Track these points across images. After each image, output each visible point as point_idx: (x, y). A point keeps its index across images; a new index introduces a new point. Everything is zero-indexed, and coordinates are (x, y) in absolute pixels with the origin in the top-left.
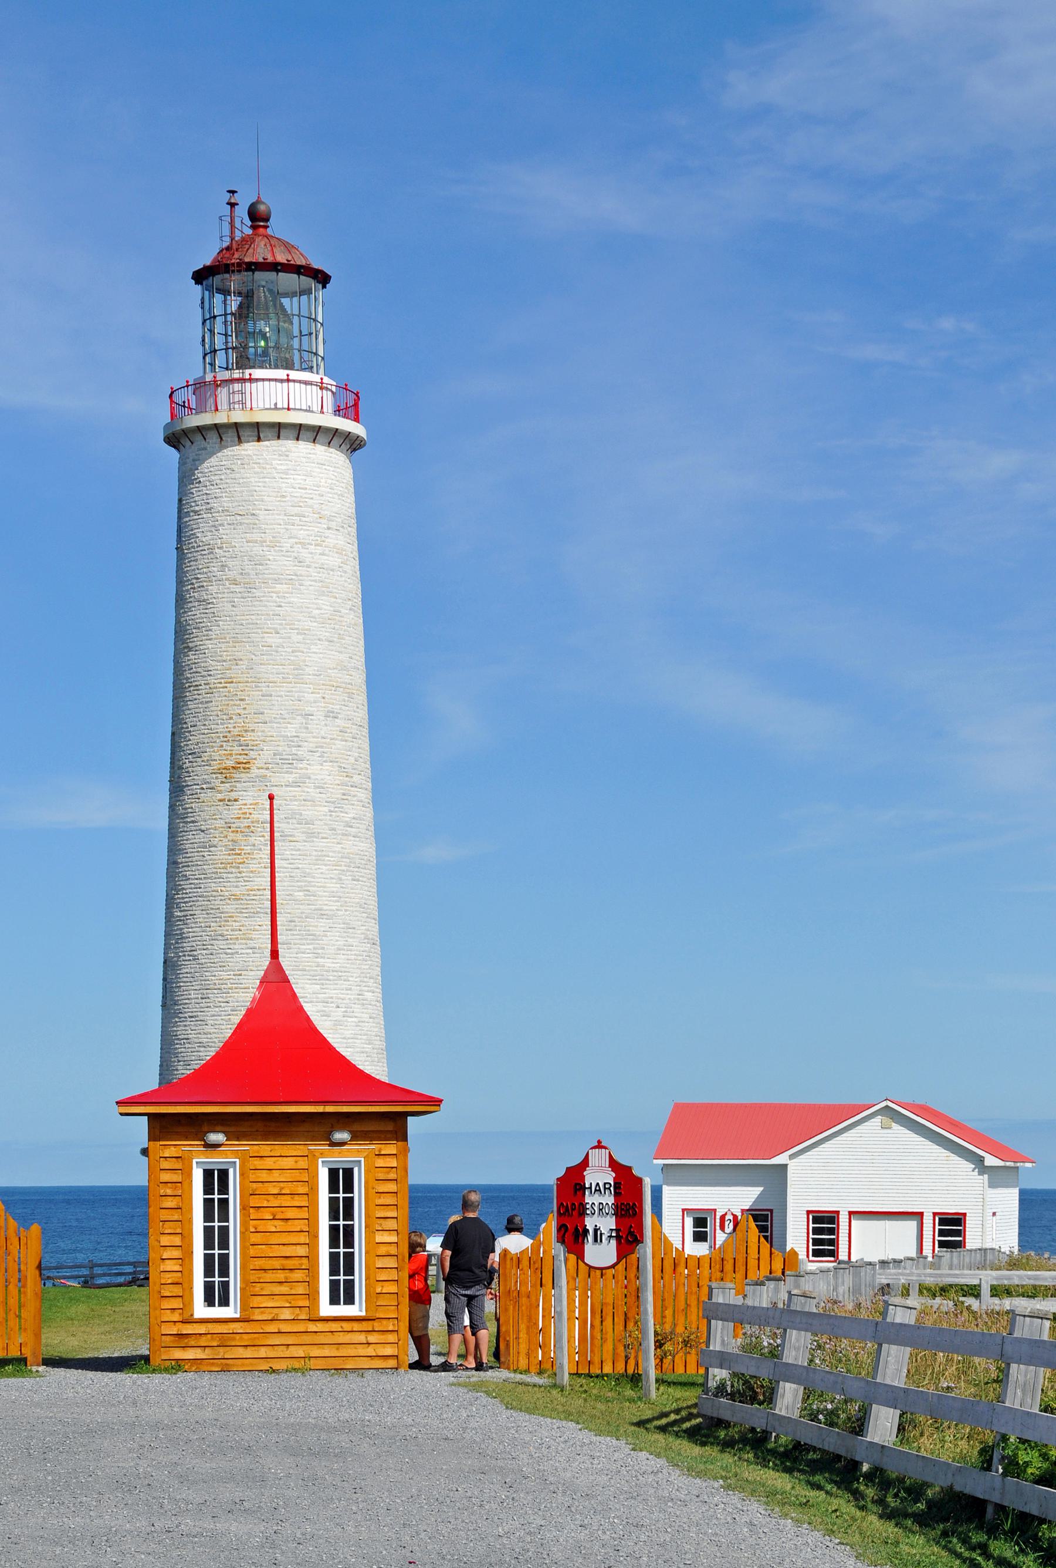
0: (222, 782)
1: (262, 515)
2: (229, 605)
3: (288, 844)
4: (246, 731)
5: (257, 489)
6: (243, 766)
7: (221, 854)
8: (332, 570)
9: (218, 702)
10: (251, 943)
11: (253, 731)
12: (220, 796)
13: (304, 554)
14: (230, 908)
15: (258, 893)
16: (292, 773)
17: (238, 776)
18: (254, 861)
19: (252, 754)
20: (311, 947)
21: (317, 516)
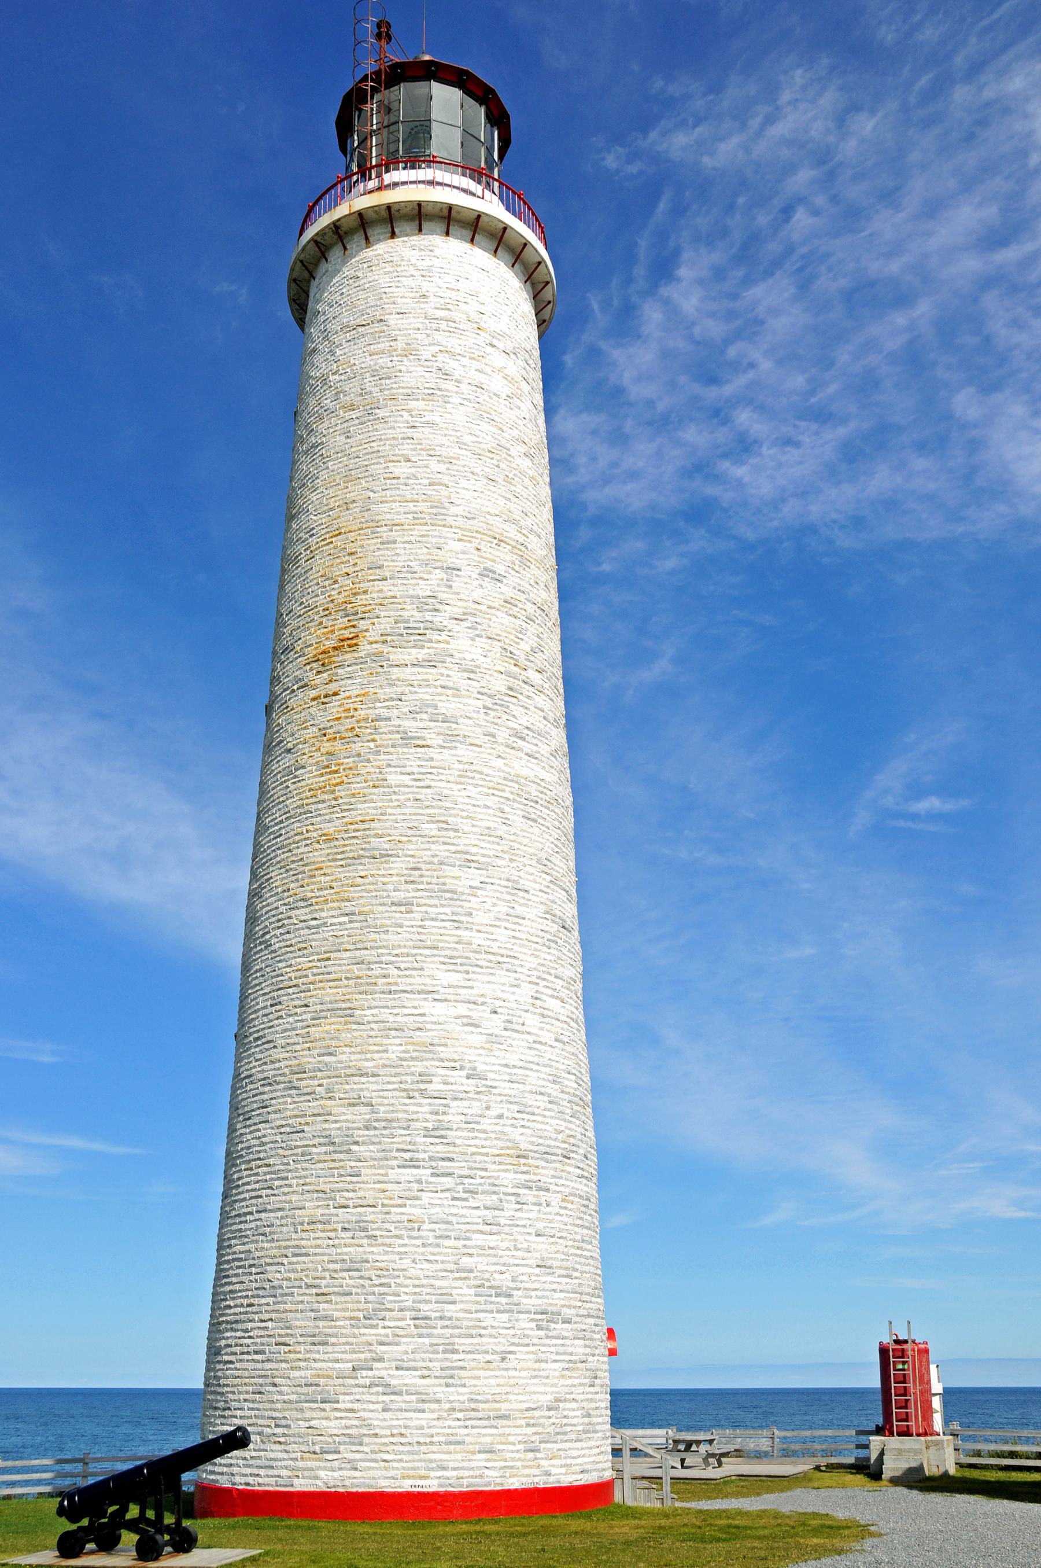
0: (319, 673)
1: (392, 320)
2: (343, 438)
3: (413, 750)
4: (355, 594)
5: (387, 290)
6: (349, 643)
7: (310, 777)
8: (498, 396)
9: (320, 564)
10: (348, 907)
11: (365, 592)
12: (313, 693)
13: (451, 365)
14: (318, 855)
15: (361, 826)
16: (422, 647)
17: (340, 658)
18: (358, 779)
19: (362, 624)
20: (448, 910)
21: (475, 326)
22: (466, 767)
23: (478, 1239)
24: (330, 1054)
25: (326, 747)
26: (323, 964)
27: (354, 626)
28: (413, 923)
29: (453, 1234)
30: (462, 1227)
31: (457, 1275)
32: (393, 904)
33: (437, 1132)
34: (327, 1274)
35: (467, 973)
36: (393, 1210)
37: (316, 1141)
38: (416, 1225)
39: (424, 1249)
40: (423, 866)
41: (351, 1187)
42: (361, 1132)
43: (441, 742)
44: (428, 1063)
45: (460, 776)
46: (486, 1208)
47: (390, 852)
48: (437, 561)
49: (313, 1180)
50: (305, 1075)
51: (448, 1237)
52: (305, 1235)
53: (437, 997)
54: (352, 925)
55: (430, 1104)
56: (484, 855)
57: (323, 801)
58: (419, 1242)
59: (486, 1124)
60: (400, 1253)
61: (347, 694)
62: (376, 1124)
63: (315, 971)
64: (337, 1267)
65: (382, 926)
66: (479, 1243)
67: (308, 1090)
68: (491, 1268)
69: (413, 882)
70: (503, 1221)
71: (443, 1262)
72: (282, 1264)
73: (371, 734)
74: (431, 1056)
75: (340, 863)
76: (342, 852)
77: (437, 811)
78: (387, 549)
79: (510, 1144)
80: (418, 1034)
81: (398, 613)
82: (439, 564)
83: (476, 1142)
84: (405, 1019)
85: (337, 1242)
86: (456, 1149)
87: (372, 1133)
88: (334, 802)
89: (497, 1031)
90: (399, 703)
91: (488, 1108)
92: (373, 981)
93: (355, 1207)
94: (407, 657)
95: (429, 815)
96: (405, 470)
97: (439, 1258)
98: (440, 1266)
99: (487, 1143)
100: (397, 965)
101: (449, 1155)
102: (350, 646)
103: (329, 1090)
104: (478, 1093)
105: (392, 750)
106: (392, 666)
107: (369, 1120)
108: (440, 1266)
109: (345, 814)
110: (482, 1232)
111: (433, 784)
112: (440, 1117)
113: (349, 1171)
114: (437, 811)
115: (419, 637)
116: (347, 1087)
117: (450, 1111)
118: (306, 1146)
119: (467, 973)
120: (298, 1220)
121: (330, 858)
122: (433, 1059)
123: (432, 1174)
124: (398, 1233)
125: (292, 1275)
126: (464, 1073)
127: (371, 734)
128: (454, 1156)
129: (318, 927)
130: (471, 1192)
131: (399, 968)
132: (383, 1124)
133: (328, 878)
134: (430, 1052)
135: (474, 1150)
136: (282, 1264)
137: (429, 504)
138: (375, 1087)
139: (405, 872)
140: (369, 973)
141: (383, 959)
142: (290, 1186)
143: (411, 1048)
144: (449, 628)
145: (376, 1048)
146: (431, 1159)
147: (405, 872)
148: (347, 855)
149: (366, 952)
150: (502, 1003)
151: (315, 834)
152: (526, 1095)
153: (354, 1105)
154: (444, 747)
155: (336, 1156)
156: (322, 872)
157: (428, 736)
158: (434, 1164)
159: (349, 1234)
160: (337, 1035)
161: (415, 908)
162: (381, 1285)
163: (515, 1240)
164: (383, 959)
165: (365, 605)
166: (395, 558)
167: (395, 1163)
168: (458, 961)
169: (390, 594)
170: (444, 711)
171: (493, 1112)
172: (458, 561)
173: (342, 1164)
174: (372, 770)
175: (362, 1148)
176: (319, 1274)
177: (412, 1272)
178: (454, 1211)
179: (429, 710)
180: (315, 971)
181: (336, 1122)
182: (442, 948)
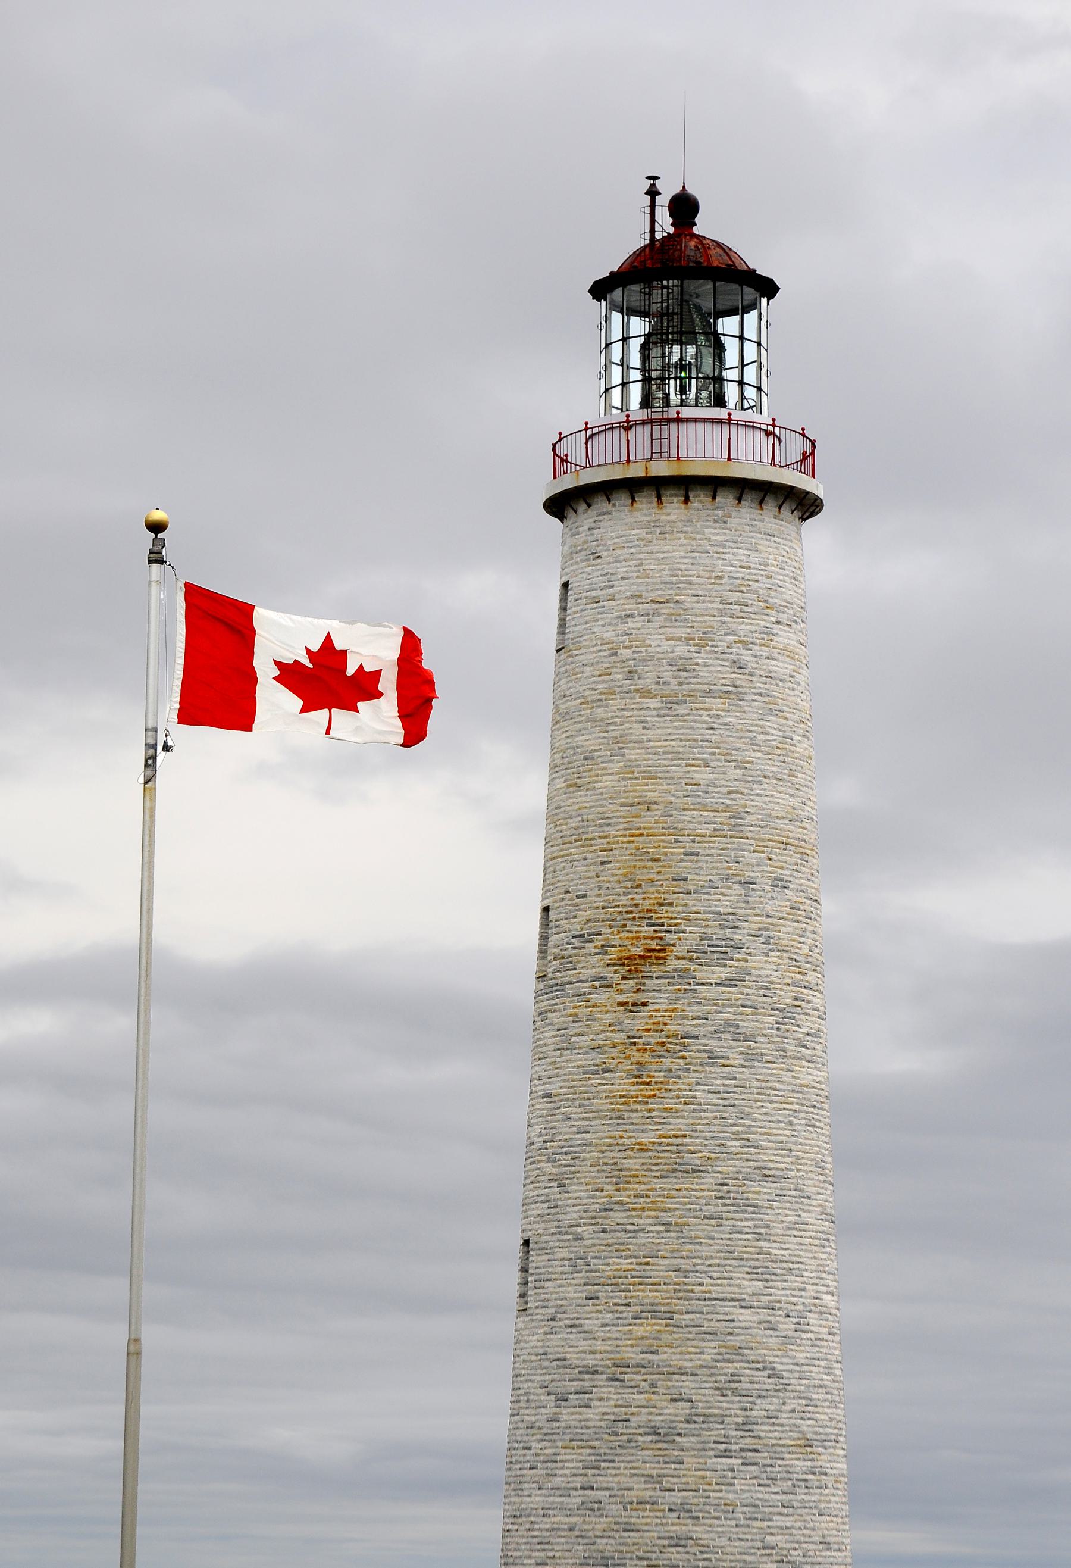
0: (624, 978)
2: (640, 726)
3: (718, 1069)
4: (661, 905)
10: (666, 1217)
13: (746, 656)
16: (725, 966)
19: (670, 938)
22: (763, 1084)
23: (779, 1521)
24: (652, 1352)
25: (637, 1057)
26: (644, 1267)
27: (661, 938)
28: (723, 1236)
29: (759, 1516)
30: (766, 1510)
31: (763, 1552)
32: (705, 1217)
33: (746, 1426)
34: (656, 1549)
35: (767, 1281)
36: (711, 1494)
37: (641, 1431)
38: (731, 1508)
39: (737, 1529)
40: (730, 1182)
41: (675, 1473)
42: (682, 1425)
43: (742, 1062)
44: (738, 1365)
45: (758, 1094)
46: (784, 1493)
47: (701, 1168)
48: (736, 875)
49: (640, 1464)
50: (628, 1370)
51: (756, 1519)
52: (634, 1513)
53: (743, 1304)
54: (669, 1234)
55: (740, 1402)
56: (778, 1169)
57: (637, 1111)
58: (734, 1523)
59: (784, 1418)
60: (717, 1532)
61: (657, 1007)
62: (695, 1418)
63: (634, 1273)
64: (666, 1542)
65: (696, 1237)
66: (779, 1524)
67: (633, 1384)
68: (788, 1546)
69: (721, 1198)
70: (796, 1504)
71: (752, 1540)
72: (614, 1538)
73: (680, 1051)
74: (740, 1358)
75: (657, 1174)
76: (657, 1164)
77: (740, 1129)
78: (690, 861)
79: (800, 1436)
80: (729, 1338)
81: (703, 930)
82: (737, 879)
83: (776, 1434)
84: (718, 1324)
85: (664, 1521)
86: (760, 1442)
87: (693, 1426)
88: (647, 1114)
89: (791, 1333)
90: (704, 1021)
91: (784, 1404)
92: (690, 1288)
93: (679, 1491)
94: (711, 976)
95: (734, 1133)
96: (705, 776)
97: (749, 1537)
98: (750, 1544)
99: (783, 1435)
100: (710, 1274)
101: (755, 1447)
102: (658, 958)
103: (652, 1385)
104: (776, 1391)
105: (700, 1068)
106: (698, 984)
107: (690, 1415)
108: (750, 1544)
109: (659, 1127)
110: (780, 1514)
111: (737, 1102)
112: (748, 1413)
113: (673, 1459)
114: (740, 1129)
115: (722, 956)
116: (669, 1383)
117: (756, 1407)
118: (634, 1434)
119: (767, 1281)
120: (626, 1500)
121: (645, 1167)
122: (742, 1361)
123: (743, 1464)
124: (717, 1514)
125: (624, 1548)
126: (766, 1373)
127: (680, 1051)
128: (759, 1447)
129: (635, 1231)
130: (772, 1479)
131: (711, 1278)
132: (701, 1419)
133: (643, 1187)
134: (739, 1354)
135: (774, 1442)
136: (614, 1538)
137: (728, 814)
138: (693, 1385)
139: (715, 1187)
140: (686, 1280)
141: (698, 1268)
142: (618, 1468)
143: (723, 1350)
144: (747, 945)
145: (693, 1350)
146: (742, 1450)
147: (715, 1187)
148: (661, 1167)
149: (682, 1261)
150: (793, 1307)
151: (627, 1141)
152: (811, 1389)
153: (675, 1400)
154: (745, 1066)
155: (660, 1445)
156: (637, 1180)
157: (731, 1056)
158: (743, 1454)
159: (676, 1515)
160: (658, 1335)
161: (724, 1222)
162: (704, 1560)
163: (805, 1521)
164: (698, 1268)
165: (671, 918)
166: (697, 871)
167: (711, 1453)
168: (759, 1270)
169: (695, 909)
170: (744, 1030)
171: (788, 1408)
172: (752, 874)
173: (666, 1452)
174: (683, 1087)
175: (684, 1439)
176: (649, 1548)
177: (728, 1550)
178: (760, 1496)
179: (732, 1029)
180: (634, 1273)
181: (660, 1414)
182: (747, 1260)
